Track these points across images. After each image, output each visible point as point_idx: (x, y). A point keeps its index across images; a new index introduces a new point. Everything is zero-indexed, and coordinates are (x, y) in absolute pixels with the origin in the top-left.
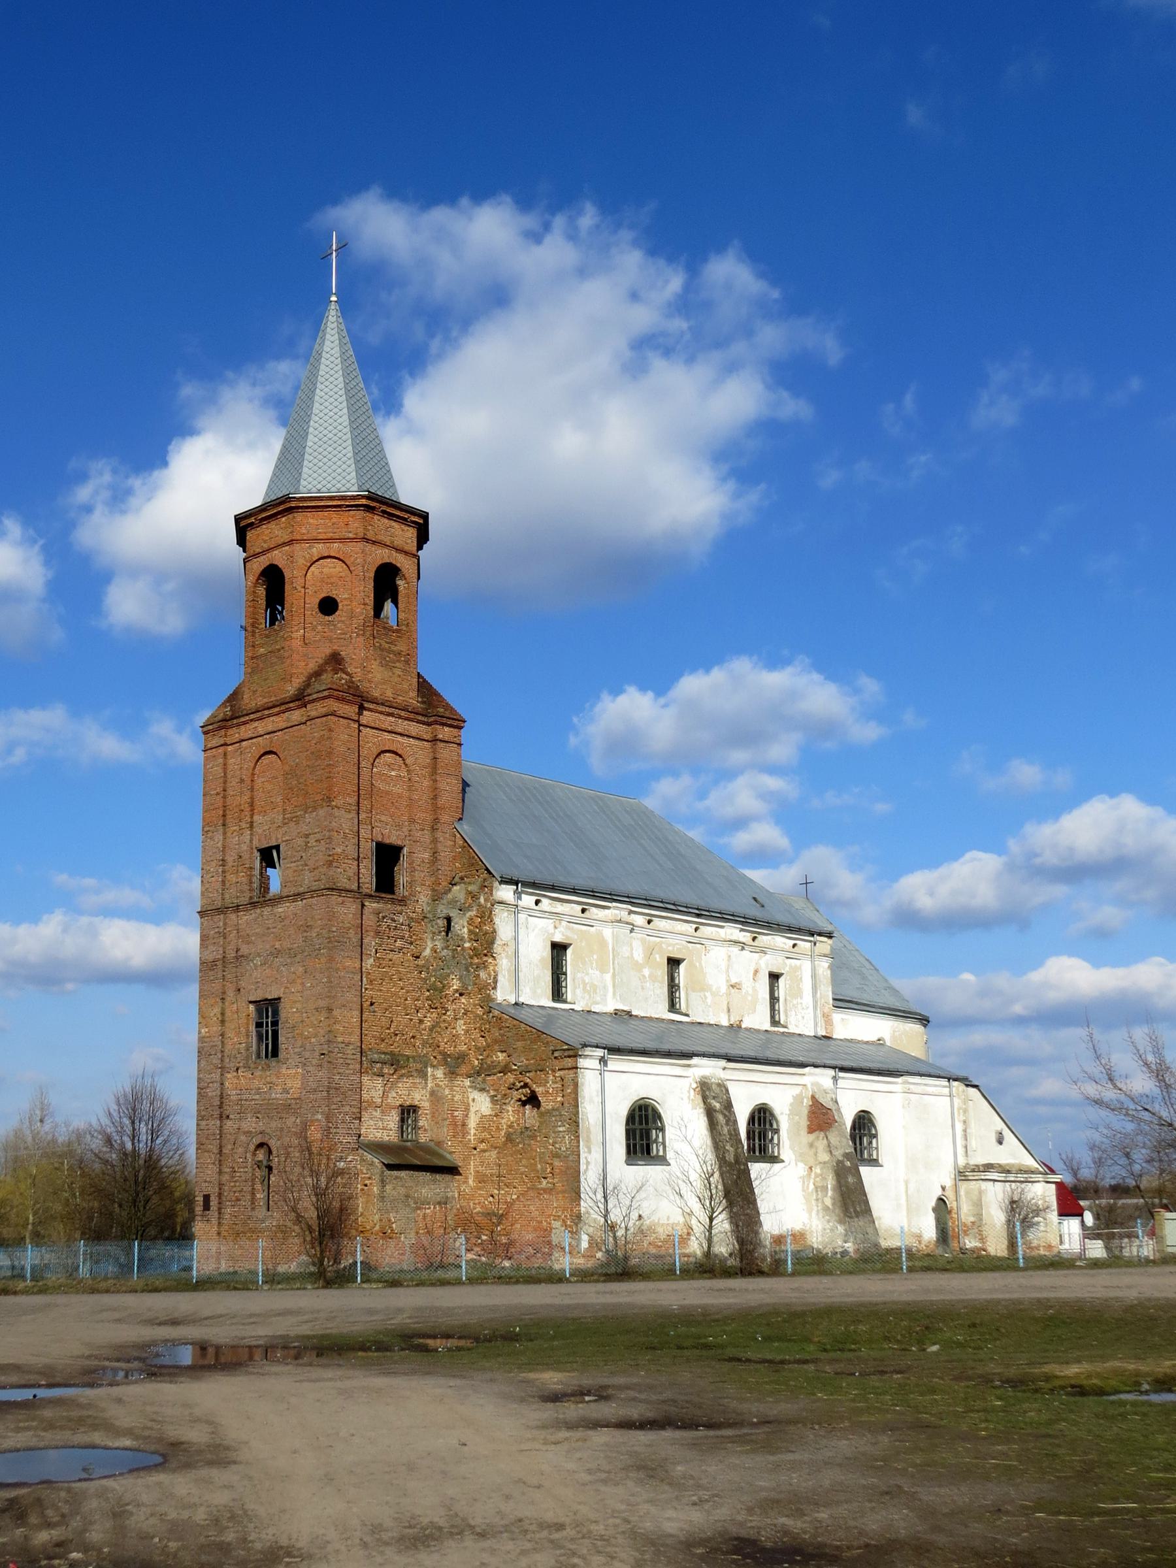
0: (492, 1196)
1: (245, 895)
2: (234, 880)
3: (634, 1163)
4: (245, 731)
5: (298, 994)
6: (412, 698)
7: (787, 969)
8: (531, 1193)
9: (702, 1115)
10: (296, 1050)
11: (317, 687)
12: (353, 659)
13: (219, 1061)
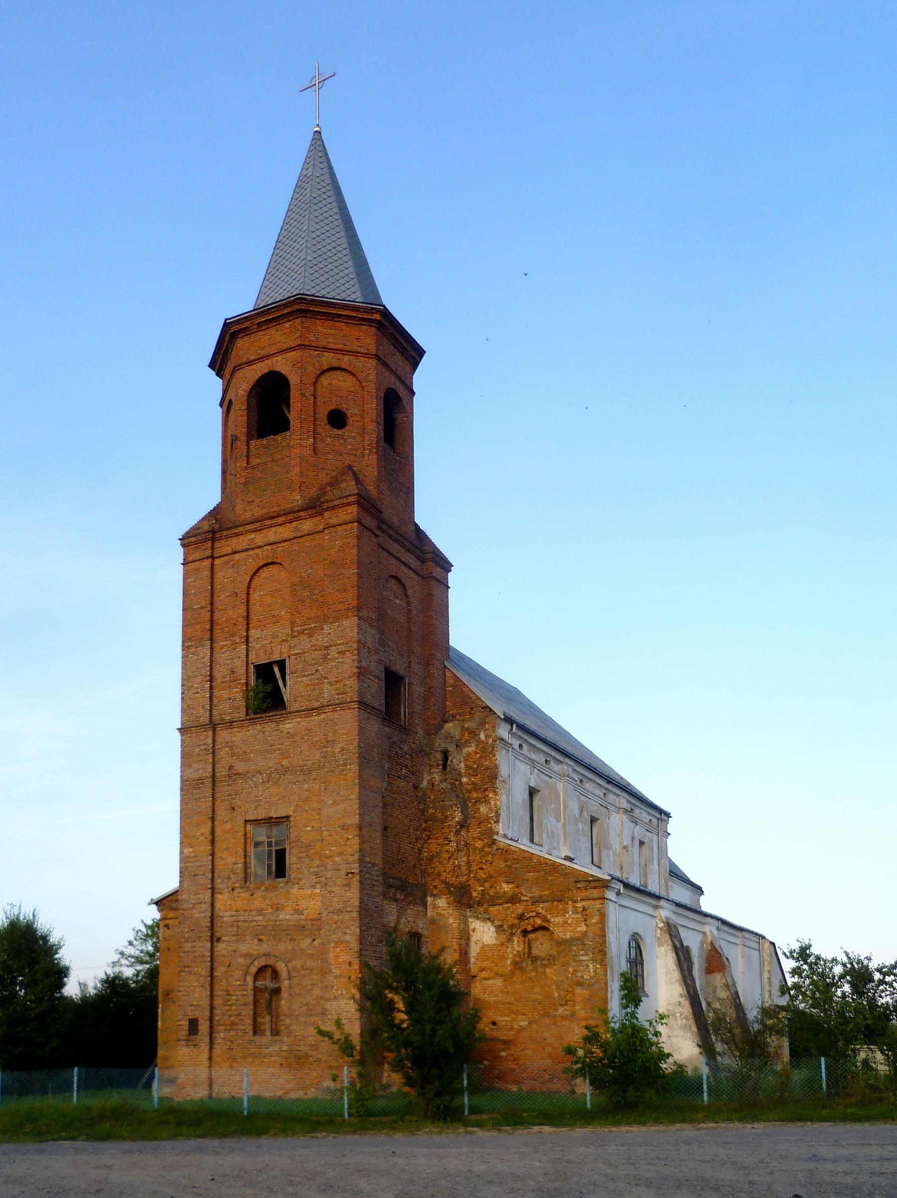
5: (314, 813)
8: (547, 1020)
9: (670, 952)
10: (312, 870)
12: (366, 476)
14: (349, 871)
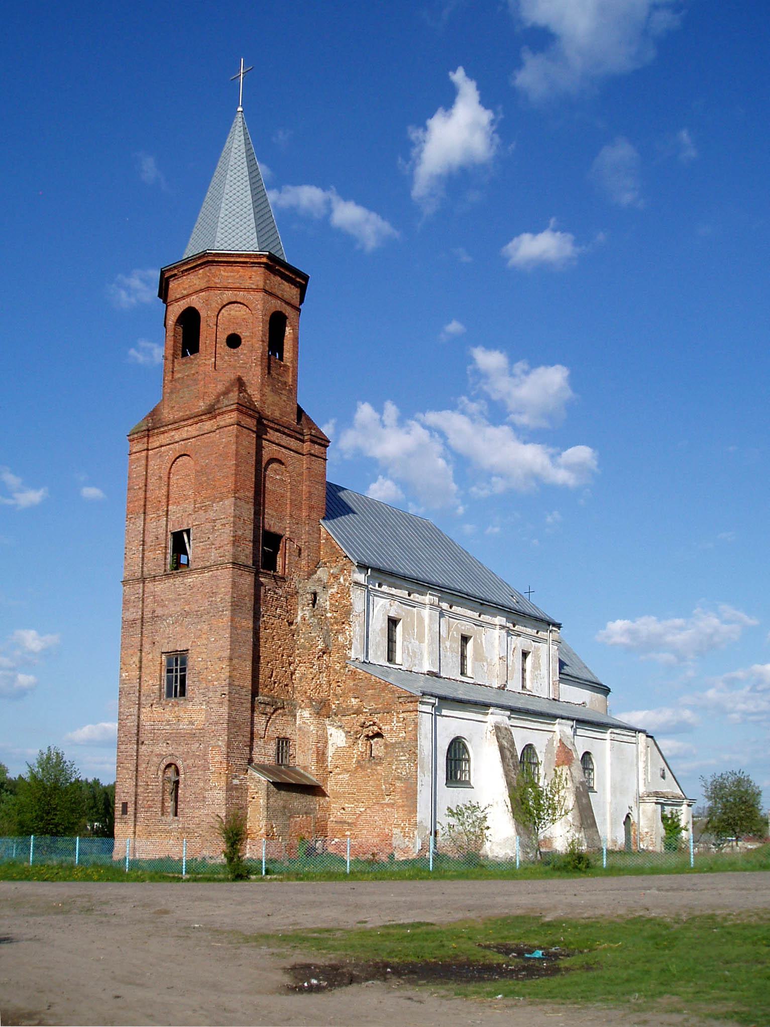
0: (344, 809)
1: (160, 568)
2: (152, 556)
3: (458, 786)
4: (163, 439)
6: (292, 419)
7: (533, 649)
8: (377, 807)
10: (201, 691)
11: (226, 402)
12: (252, 384)
13: (137, 699)
14: (223, 692)
